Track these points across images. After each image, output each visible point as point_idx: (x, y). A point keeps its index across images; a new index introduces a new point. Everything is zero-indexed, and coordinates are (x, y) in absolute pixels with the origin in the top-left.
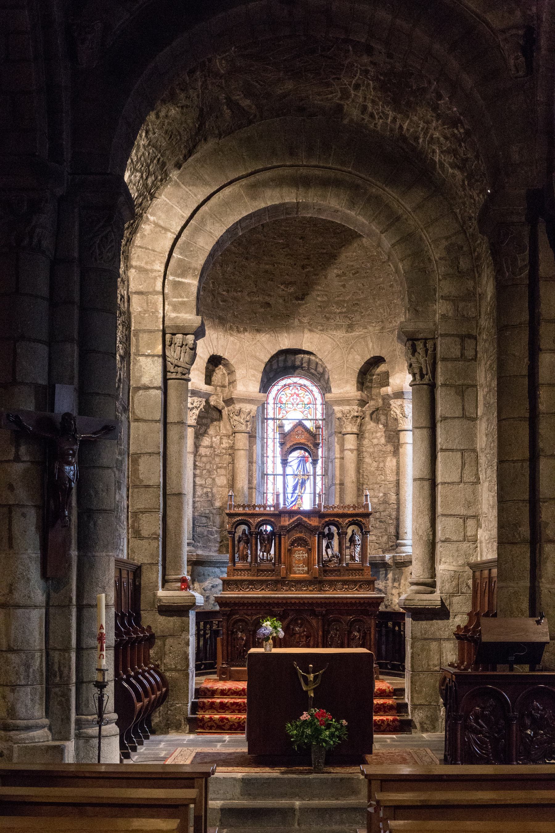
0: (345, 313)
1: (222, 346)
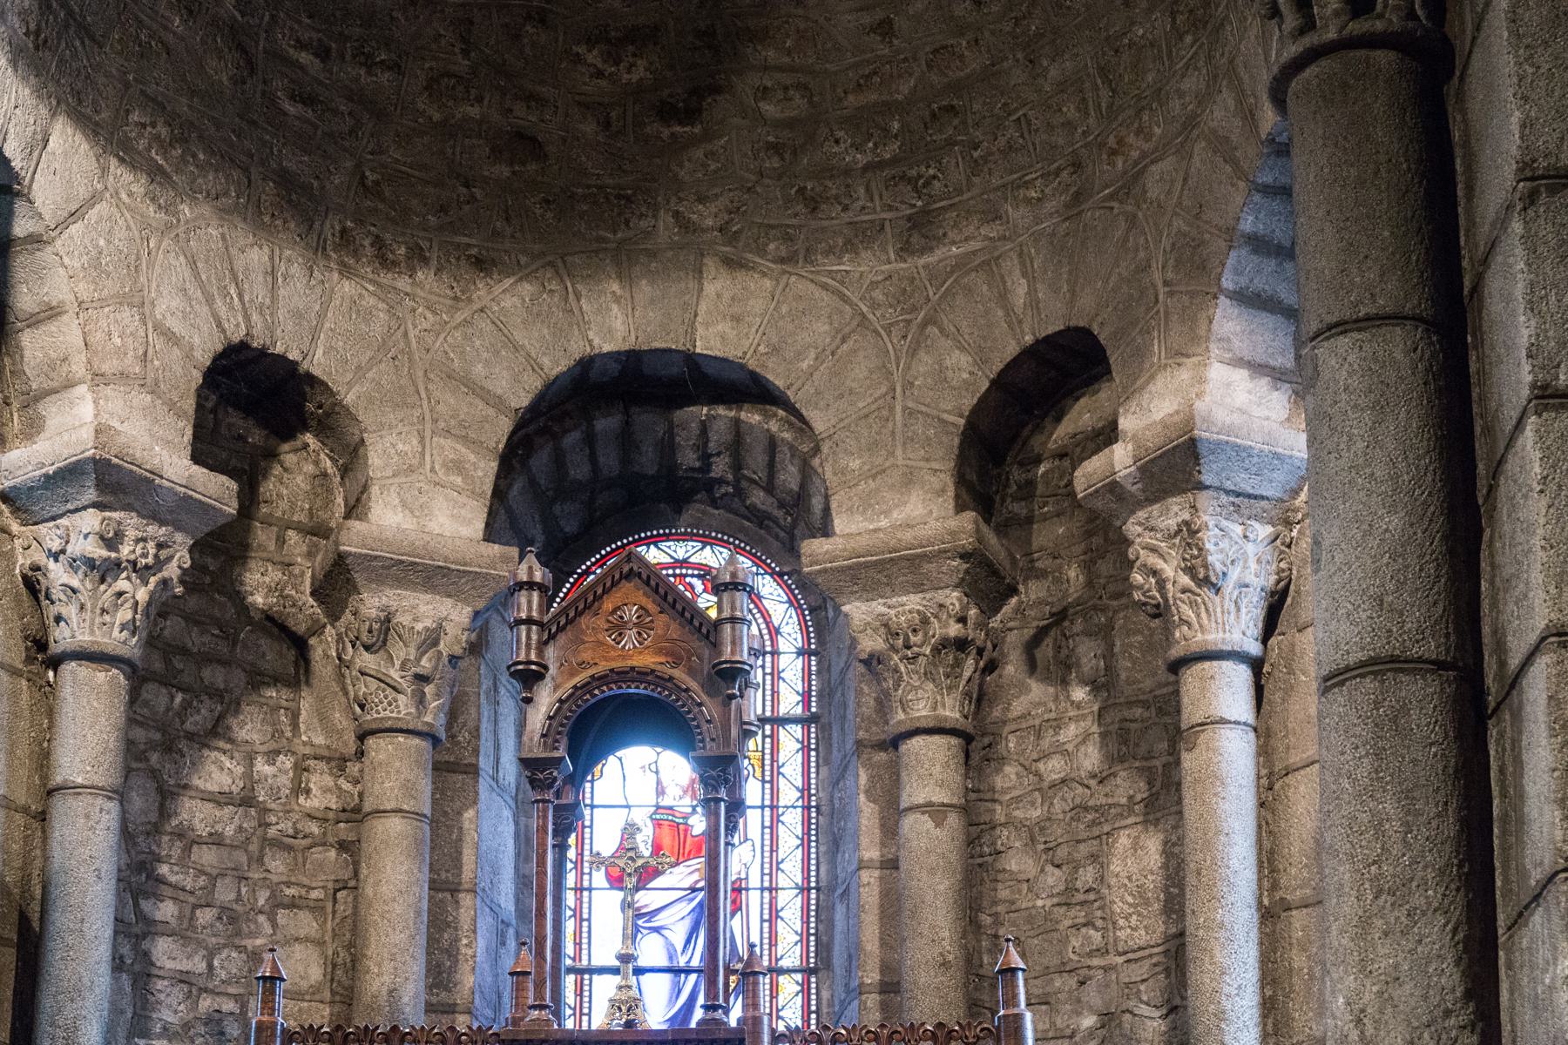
0: (894, 161)
1: (298, 315)
